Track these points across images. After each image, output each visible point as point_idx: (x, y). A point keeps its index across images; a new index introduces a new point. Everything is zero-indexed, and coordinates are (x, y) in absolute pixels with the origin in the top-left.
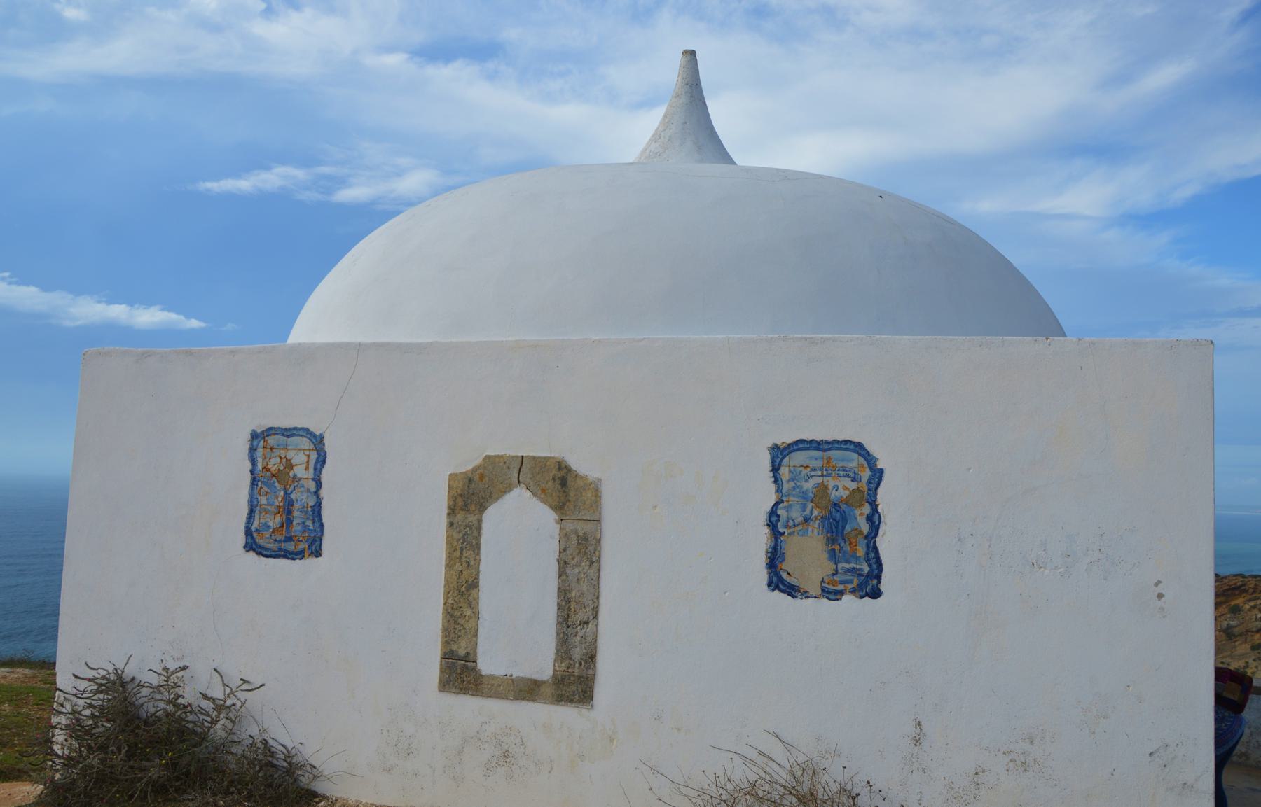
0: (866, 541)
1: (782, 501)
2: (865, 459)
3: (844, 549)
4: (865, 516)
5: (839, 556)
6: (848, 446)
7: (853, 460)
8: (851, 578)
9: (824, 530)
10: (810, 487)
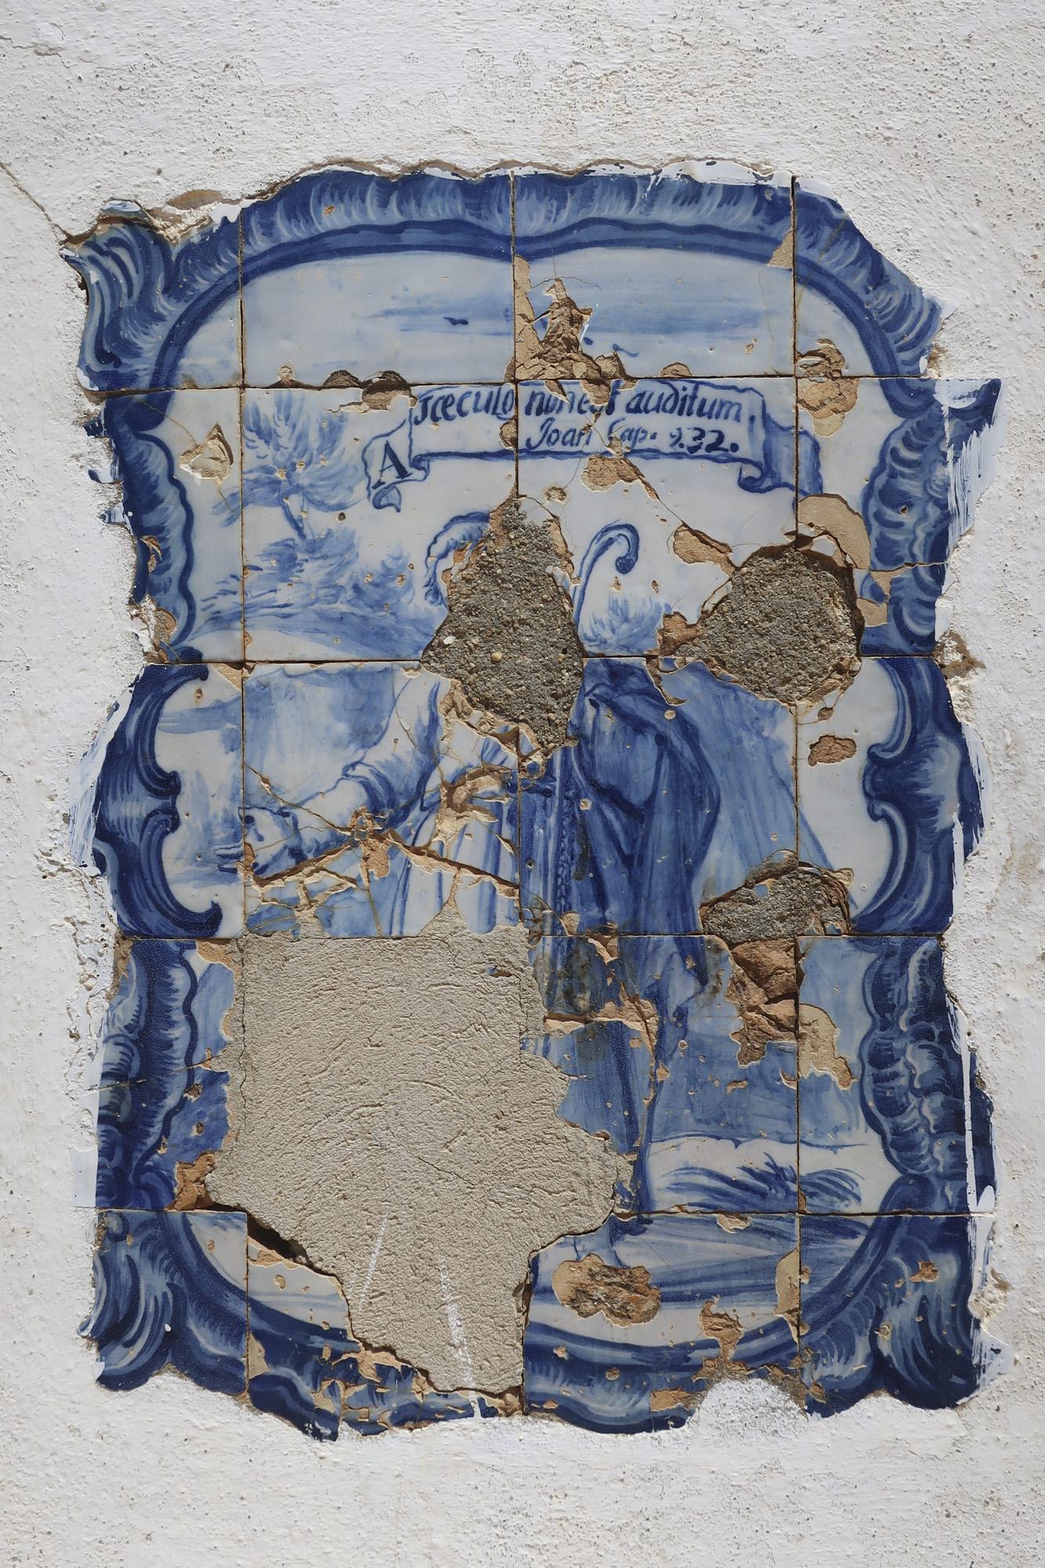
0: (863, 961)
1: (195, 667)
2: (851, 308)
3: (694, 1025)
4: (857, 762)
5: (657, 1086)
7: (751, 319)
8: (760, 1249)
9: (536, 887)
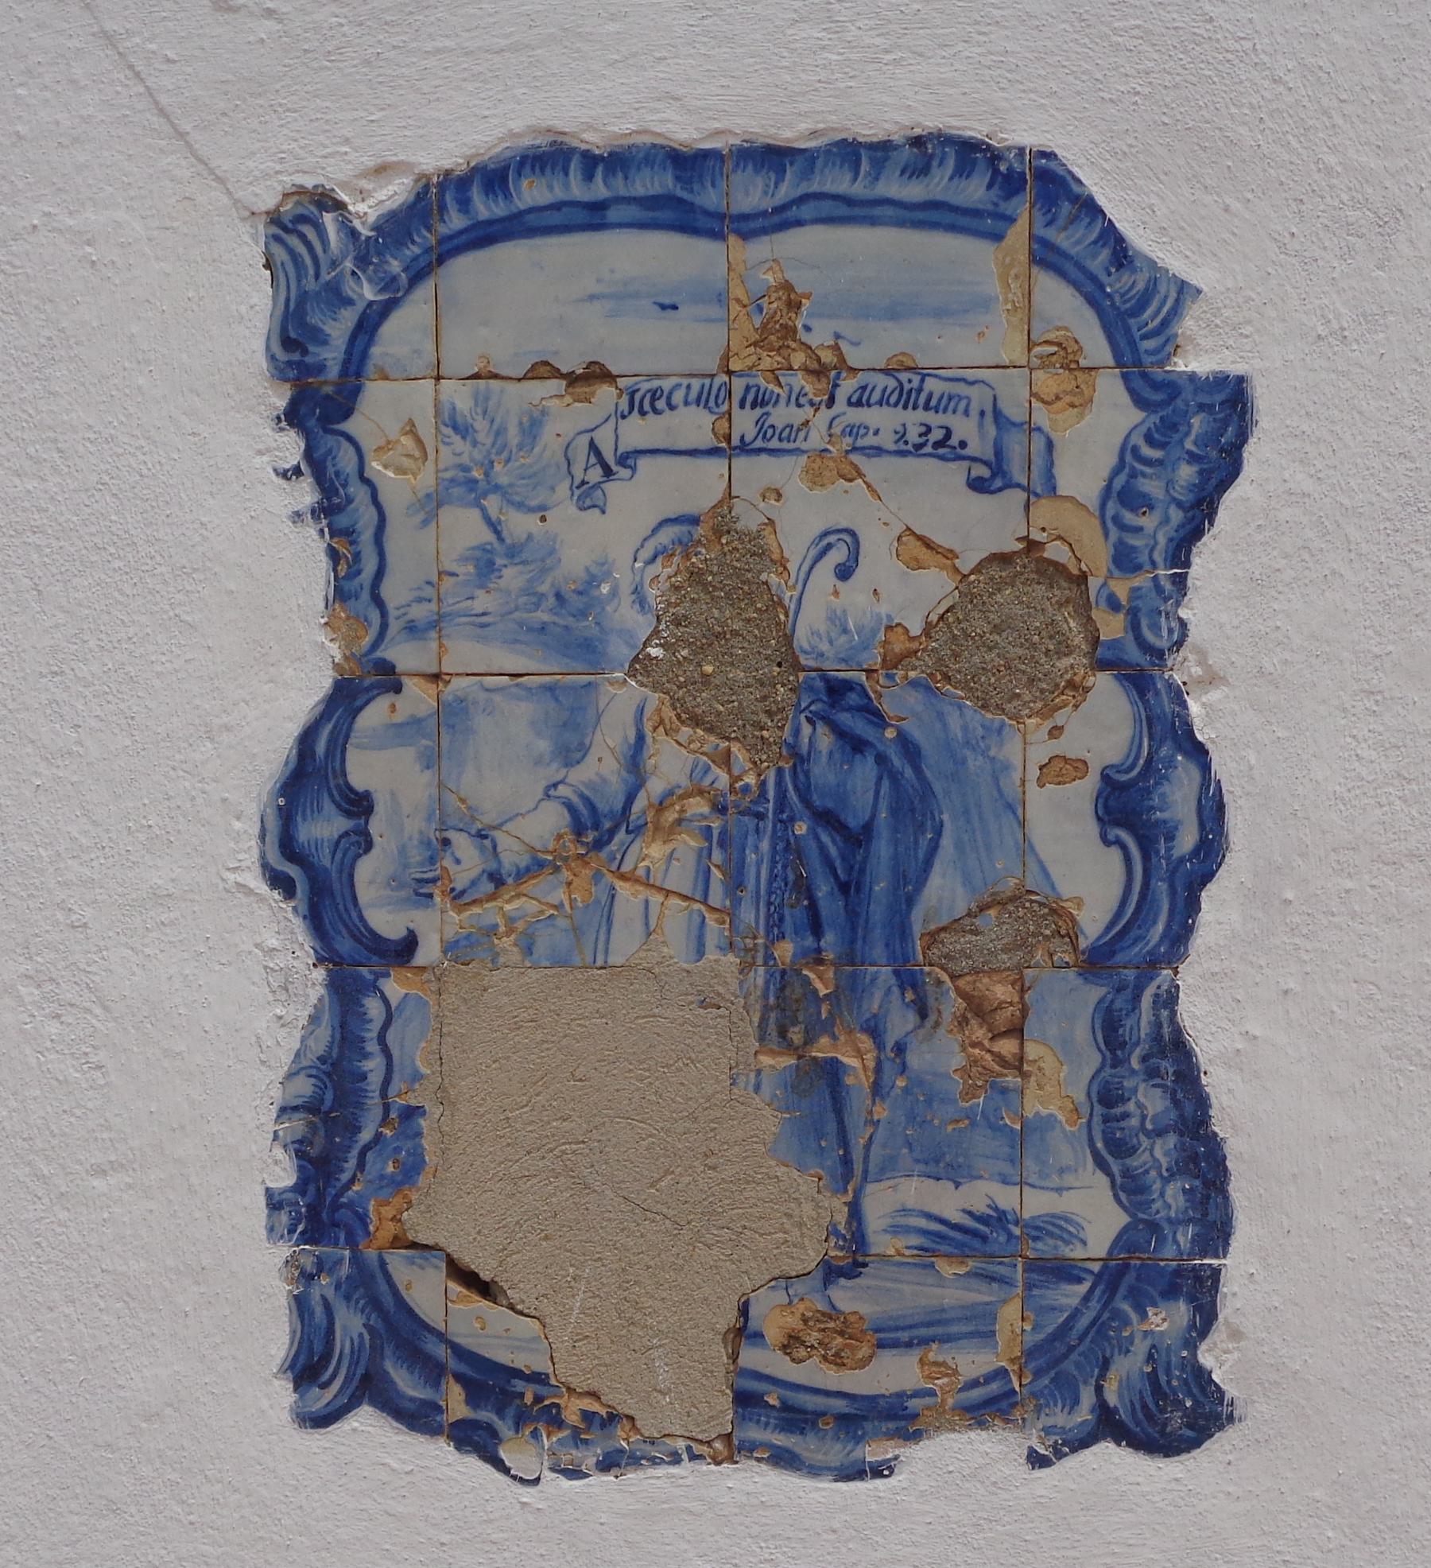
0: (1094, 993)
2: (1094, 296)
3: (913, 1060)
4: (1090, 784)
6: (938, 185)
9: (748, 915)
10: (621, 556)
